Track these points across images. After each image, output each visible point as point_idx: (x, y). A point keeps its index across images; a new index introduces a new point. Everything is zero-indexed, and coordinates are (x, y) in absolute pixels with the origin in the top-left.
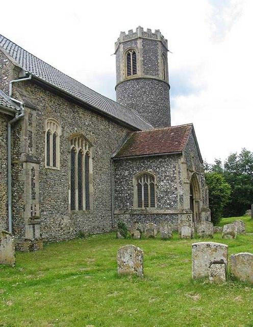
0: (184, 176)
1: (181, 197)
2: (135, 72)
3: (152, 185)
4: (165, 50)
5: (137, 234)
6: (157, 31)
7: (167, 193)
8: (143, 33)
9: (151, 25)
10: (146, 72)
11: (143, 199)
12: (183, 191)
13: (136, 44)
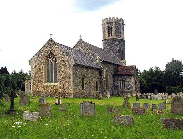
0: (133, 81)
1: (133, 87)
2: (112, 35)
3: (124, 83)
4: (123, 25)
5: (122, 95)
6: (121, 19)
7: (128, 85)
8: (115, 20)
9: (118, 16)
10: (116, 36)
11: (50, 73)
12: (133, 85)
13: (112, 24)
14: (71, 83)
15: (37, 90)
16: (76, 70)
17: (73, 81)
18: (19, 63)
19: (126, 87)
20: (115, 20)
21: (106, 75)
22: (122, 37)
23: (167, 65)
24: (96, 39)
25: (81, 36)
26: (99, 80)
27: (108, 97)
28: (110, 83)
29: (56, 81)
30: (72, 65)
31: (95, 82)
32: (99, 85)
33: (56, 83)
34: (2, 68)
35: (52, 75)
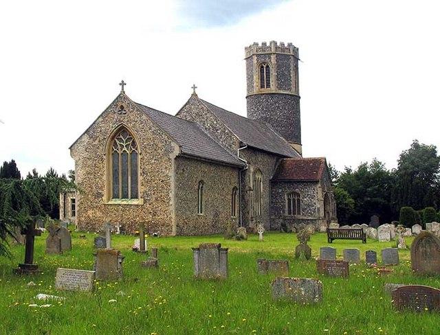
0: (320, 195)
1: (319, 209)
2: (268, 85)
3: (299, 200)
4: (297, 59)
5: (294, 230)
6: (290, 45)
7: (309, 206)
8: (277, 48)
9: (283, 38)
10: (280, 87)
11: (120, 177)
13: (270, 58)
14: (170, 199)
15: (89, 217)
16: (183, 170)
17: (176, 195)
18: (45, 152)
19: (304, 210)
20: (277, 48)
21: (255, 180)
22: (293, 89)
23: (402, 156)
24: (231, 93)
25: (194, 87)
26: (238, 192)
27: (261, 233)
28: (265, 200)
29: (135, 196)
30: (172, 156)
31: (229, 197)
32: (237, 205)
33: (135, 200)
34: (5, 164)
35: (125, 182)
